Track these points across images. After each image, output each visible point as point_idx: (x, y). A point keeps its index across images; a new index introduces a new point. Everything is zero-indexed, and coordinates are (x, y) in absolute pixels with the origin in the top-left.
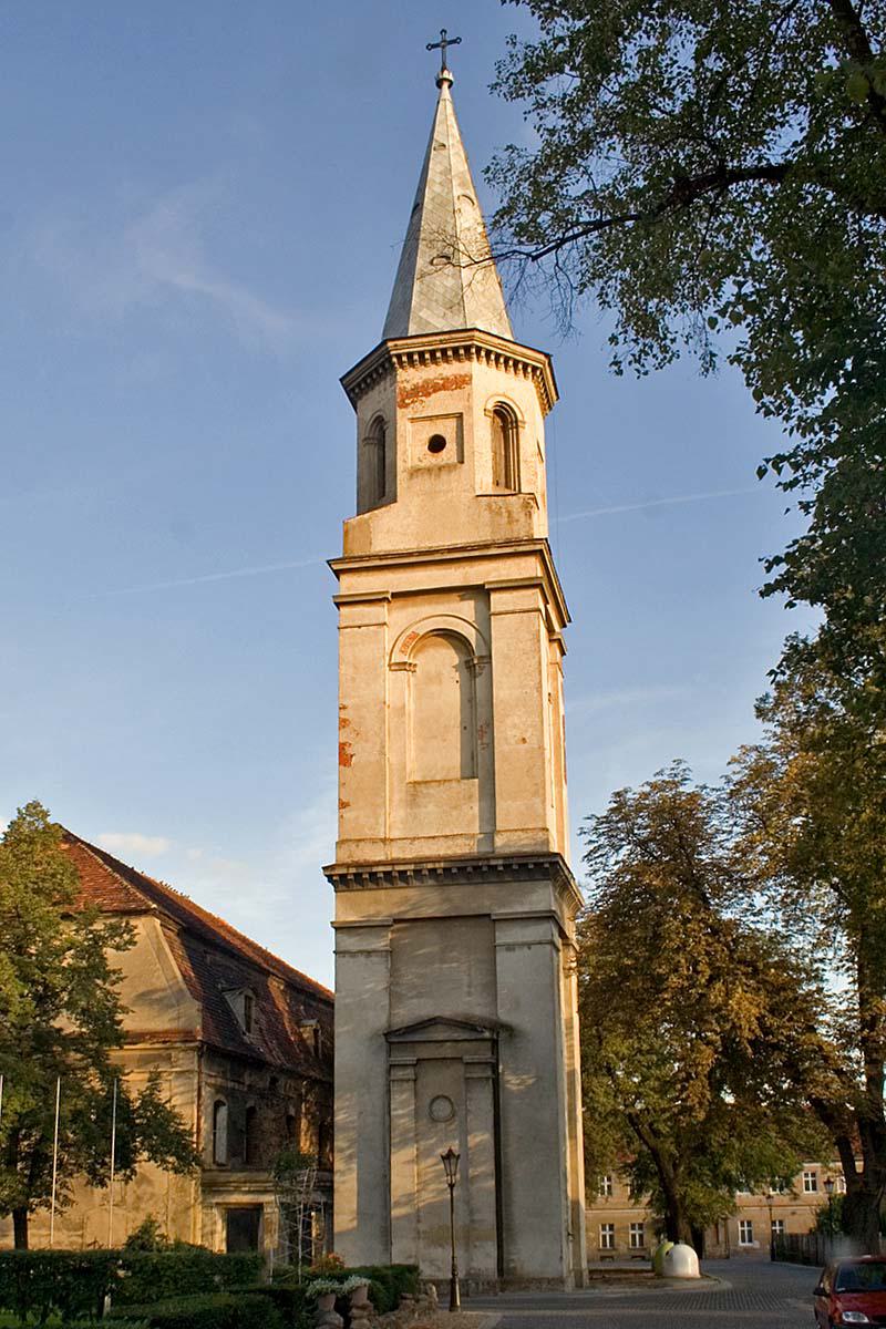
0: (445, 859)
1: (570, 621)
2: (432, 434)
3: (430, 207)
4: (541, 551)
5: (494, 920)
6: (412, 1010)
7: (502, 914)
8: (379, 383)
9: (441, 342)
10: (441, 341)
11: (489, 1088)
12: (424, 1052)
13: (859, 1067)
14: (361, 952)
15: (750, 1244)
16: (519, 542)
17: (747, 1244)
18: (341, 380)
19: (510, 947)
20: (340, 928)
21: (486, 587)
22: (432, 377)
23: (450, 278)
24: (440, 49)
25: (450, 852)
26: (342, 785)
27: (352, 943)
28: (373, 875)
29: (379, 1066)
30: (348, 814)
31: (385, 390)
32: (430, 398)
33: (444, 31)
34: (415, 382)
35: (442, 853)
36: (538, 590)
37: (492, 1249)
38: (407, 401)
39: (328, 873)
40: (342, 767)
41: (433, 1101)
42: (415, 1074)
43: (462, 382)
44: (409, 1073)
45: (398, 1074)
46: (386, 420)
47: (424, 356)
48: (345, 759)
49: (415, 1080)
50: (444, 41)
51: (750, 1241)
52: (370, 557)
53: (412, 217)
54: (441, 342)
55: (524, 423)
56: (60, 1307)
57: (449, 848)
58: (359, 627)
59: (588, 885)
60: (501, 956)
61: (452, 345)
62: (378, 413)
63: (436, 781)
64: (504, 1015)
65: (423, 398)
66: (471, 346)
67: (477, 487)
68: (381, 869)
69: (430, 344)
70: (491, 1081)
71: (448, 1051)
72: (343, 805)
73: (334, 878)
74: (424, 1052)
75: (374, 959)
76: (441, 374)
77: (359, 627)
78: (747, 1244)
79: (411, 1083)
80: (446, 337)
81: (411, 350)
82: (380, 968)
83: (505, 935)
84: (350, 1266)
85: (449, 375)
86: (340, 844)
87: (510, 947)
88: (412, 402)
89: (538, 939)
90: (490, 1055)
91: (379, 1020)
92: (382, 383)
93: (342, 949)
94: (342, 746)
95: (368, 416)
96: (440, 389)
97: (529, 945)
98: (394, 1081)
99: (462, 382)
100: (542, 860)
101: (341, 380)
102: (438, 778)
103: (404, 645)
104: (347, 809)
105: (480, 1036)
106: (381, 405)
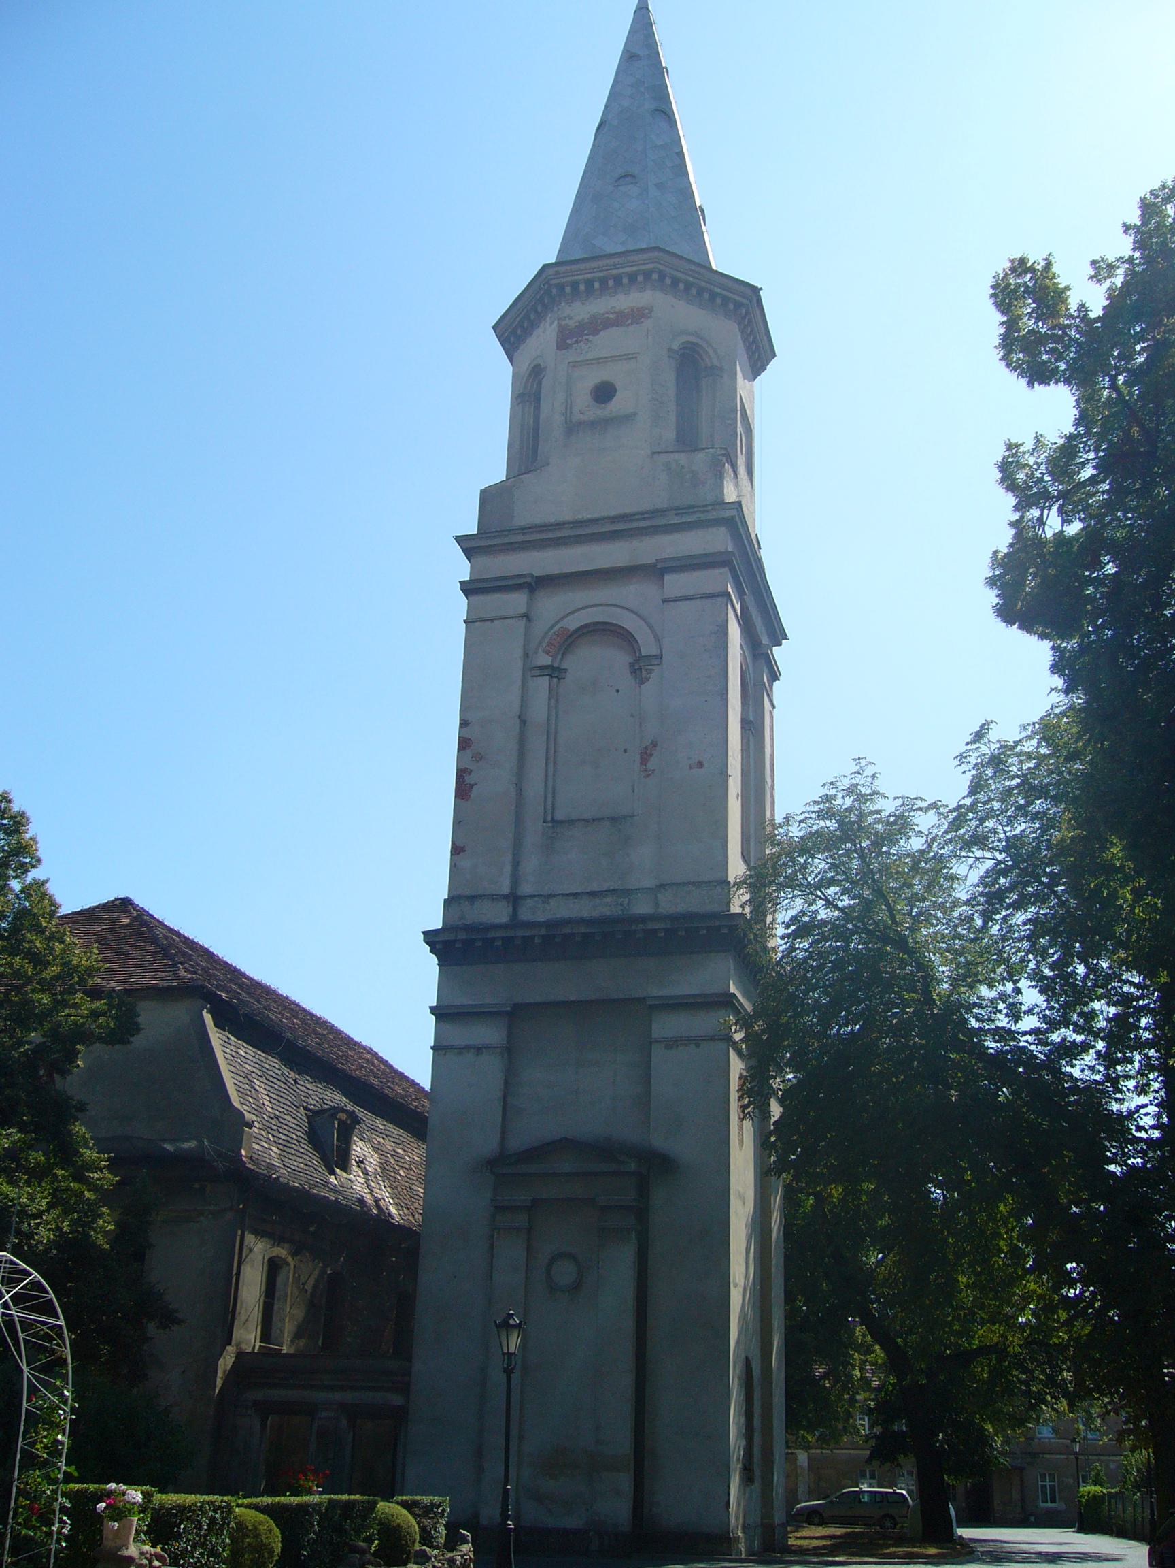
0: (590, 922)
2: (597, 381)
4: (733, 518)
7: (662, 997)
13: (224, 1551)
14: (468, 1048)
15: (1053, 1505)
17: (1049, 1505)
19: (672, 1043)
27: (461, 1035)
36: (726, 569)
37: (625, 1482)
38: (569, 341)
41: (553, 1260)
49: (529, 1230)
51: (1053, 1501)
52: (512, 531)
54: (615, 266)
56: (808, 1433)
58: (492, 620)
62: (535, 363)
63: (584, 820)
64: (658, 1142)
65: (590, 337)
68: (499, 934)
70: (634, 1235)
77: (492, 620)
78: (1049, 1505)
83: (665, 1026)
84: (525, 919)
87: (672, 1043)
88: (577, 342)
92: (542, 325)
95: (525, 366)
99: (638, 315)
102: (586, 816)
103: (550, 644)
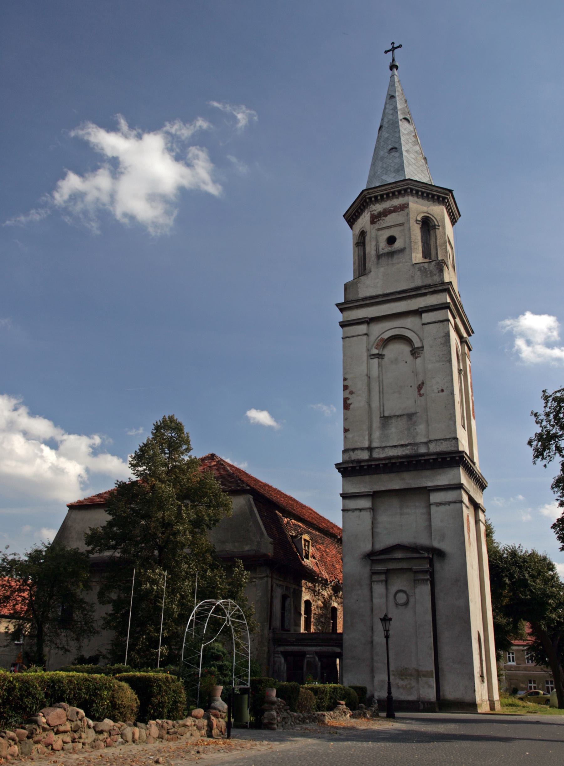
1: (473, 332)
2: (388, 235)
3: (387, 126)
5: (429, 490)
6: (385, 541)
8: (362, 214)
9: (392, 188)
10: (392, 187)
11: (428, 588)
12: (391, 566)
16: (435, 285)
18: (344, 216)
19: (438, 504)
20: (345, 496)
21: (420, 310)
22: (388, 207)
23: (397, 158)
24: (391, 52)
25: (404, 453)
26: (345, 419)
27: (353, 504)
28: (361, 467)
29: (366, 571)
30: (350, 435)
31: (365, 217)
32: (387, 218)
33: (393, 43)
34: (379, 210)
35: (400, 454)
38: (375, 220)
39: (339, 467)
40: (346, 411)
42: (386, 578)
43: (404, 207)
44: (383, 577)
45: (375, 578)
46: (365, 231)
47: (383, 196)
48: (346, 406)
50: (393, 48)
53: (379, 133)
55: (439, 226)
57: (403, 451)
59: (231, 512)
60: (433, 509)
61: (398, 189)
65: (384, 218)
66: (407, 189)
67: (413, 259)
69: (386, 190)
70: (429, 582)
71: (404, 565)
72: (346, 430)
73: (341, 470)
74: (391, 566)
75: (363, 513)
76: (392, 205)
79: (384, 583)
80: (394, 185)
81: (377, 194)
82: (367, 517)
83: (435, 497)
85: (396, 204)
86: (344, 452)
87: (438, 504)
89: (454, 500)
90: (428, 566)
91: (367, 547)
93: (346, 508)
94: (345, 400)
96: (392, 212)
97: (449, 503)
98: (374, 581)
100: (454, 455)
101: (344, 216)
104: (348, 432)
105: (422, 556)
106: (363, 225)
